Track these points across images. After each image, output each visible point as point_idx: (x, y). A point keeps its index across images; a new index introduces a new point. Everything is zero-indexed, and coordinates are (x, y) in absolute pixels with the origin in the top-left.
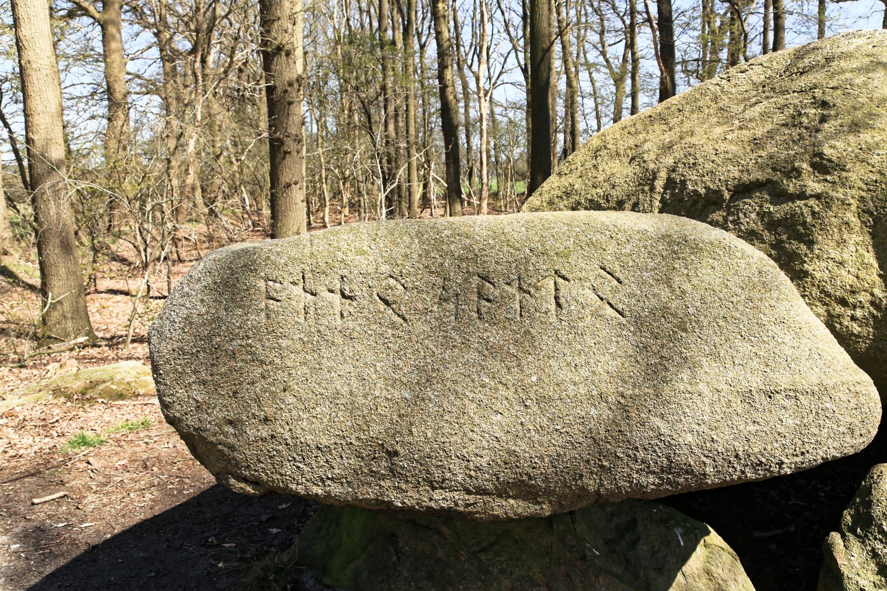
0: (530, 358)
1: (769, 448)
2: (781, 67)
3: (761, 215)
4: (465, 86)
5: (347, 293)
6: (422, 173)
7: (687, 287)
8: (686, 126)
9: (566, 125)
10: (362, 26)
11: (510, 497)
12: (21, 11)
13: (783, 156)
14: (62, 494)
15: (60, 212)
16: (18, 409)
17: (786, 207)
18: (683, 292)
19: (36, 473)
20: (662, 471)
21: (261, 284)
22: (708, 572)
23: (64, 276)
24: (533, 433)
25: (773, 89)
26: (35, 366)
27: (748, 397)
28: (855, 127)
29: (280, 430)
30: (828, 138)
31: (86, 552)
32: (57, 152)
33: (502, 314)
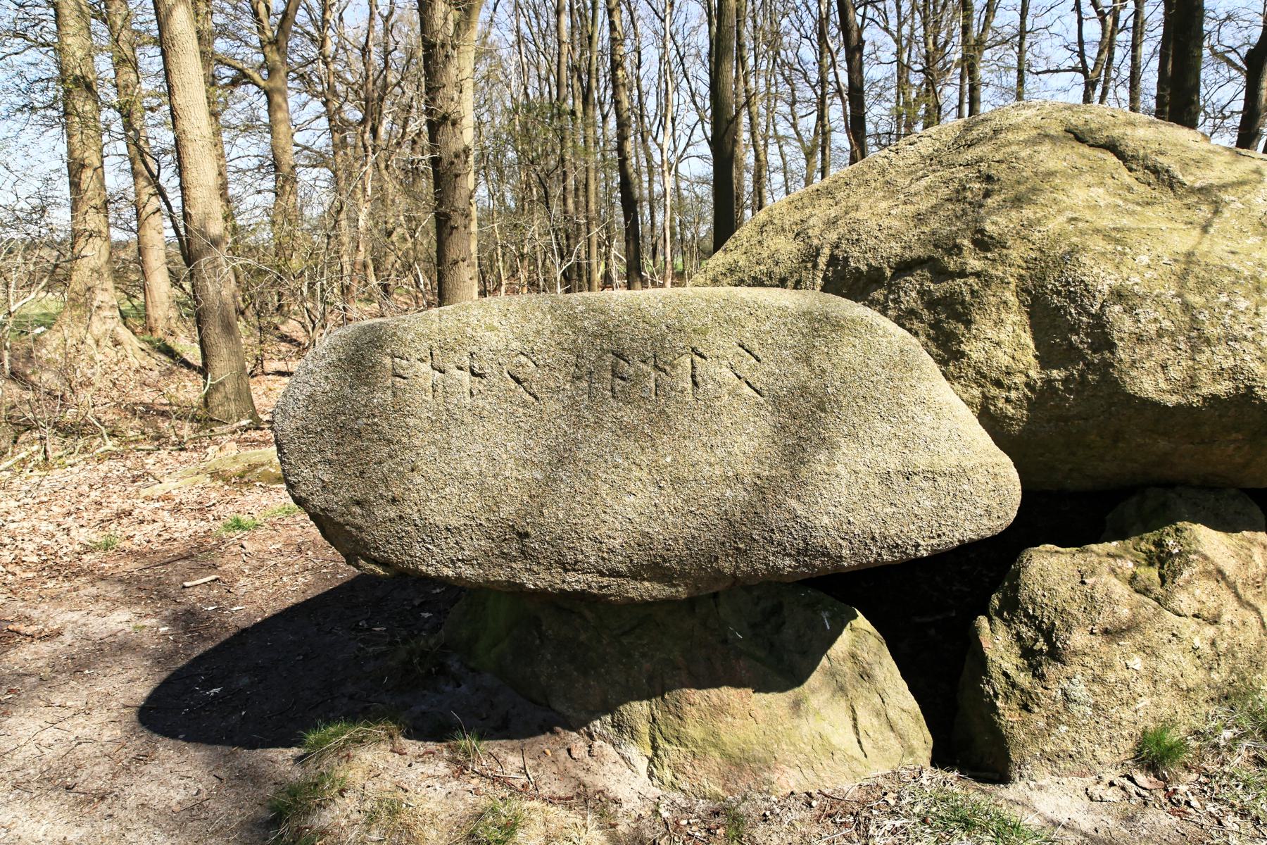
0: (665, 438)
1: (905, 530)
2: (950, 140)
3: (922, 293)
4: (649, 158)
5: (476, 370)
6: (603, 250)
7: (827, 365)
8: (853, 200)
9: (754, 201)
10: (542, 95)
11: (644, 579)
12: (175, 78)
13: (945, 232)
14: (213, 577)
15: (221, 287)
16: (174, 492)
17: (946, 285)
18: (823, 371)
19: (189, 556)
20: (799, 553)
21: (387, 361)
22: (853, 656)
23: (226, 356)
24: (667, 514)
25: (940, 162)
26: (195, 449)
27: (885, 479)
28: (1017, 202)
29: (408, 510)
30: (989, 213)
31: (235, 635)
32: (216, 227)
33: (636, 393)
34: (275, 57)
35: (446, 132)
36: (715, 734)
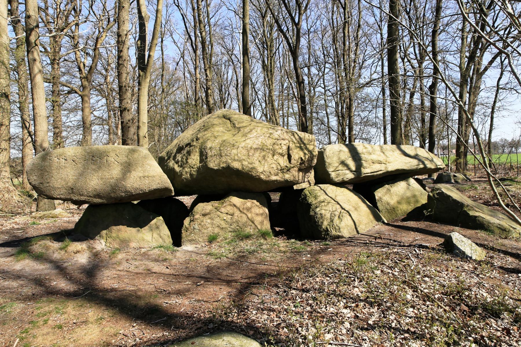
22: (156, 224)
34: (86, 83)
35: (126, 113)
36: (118, 235)
